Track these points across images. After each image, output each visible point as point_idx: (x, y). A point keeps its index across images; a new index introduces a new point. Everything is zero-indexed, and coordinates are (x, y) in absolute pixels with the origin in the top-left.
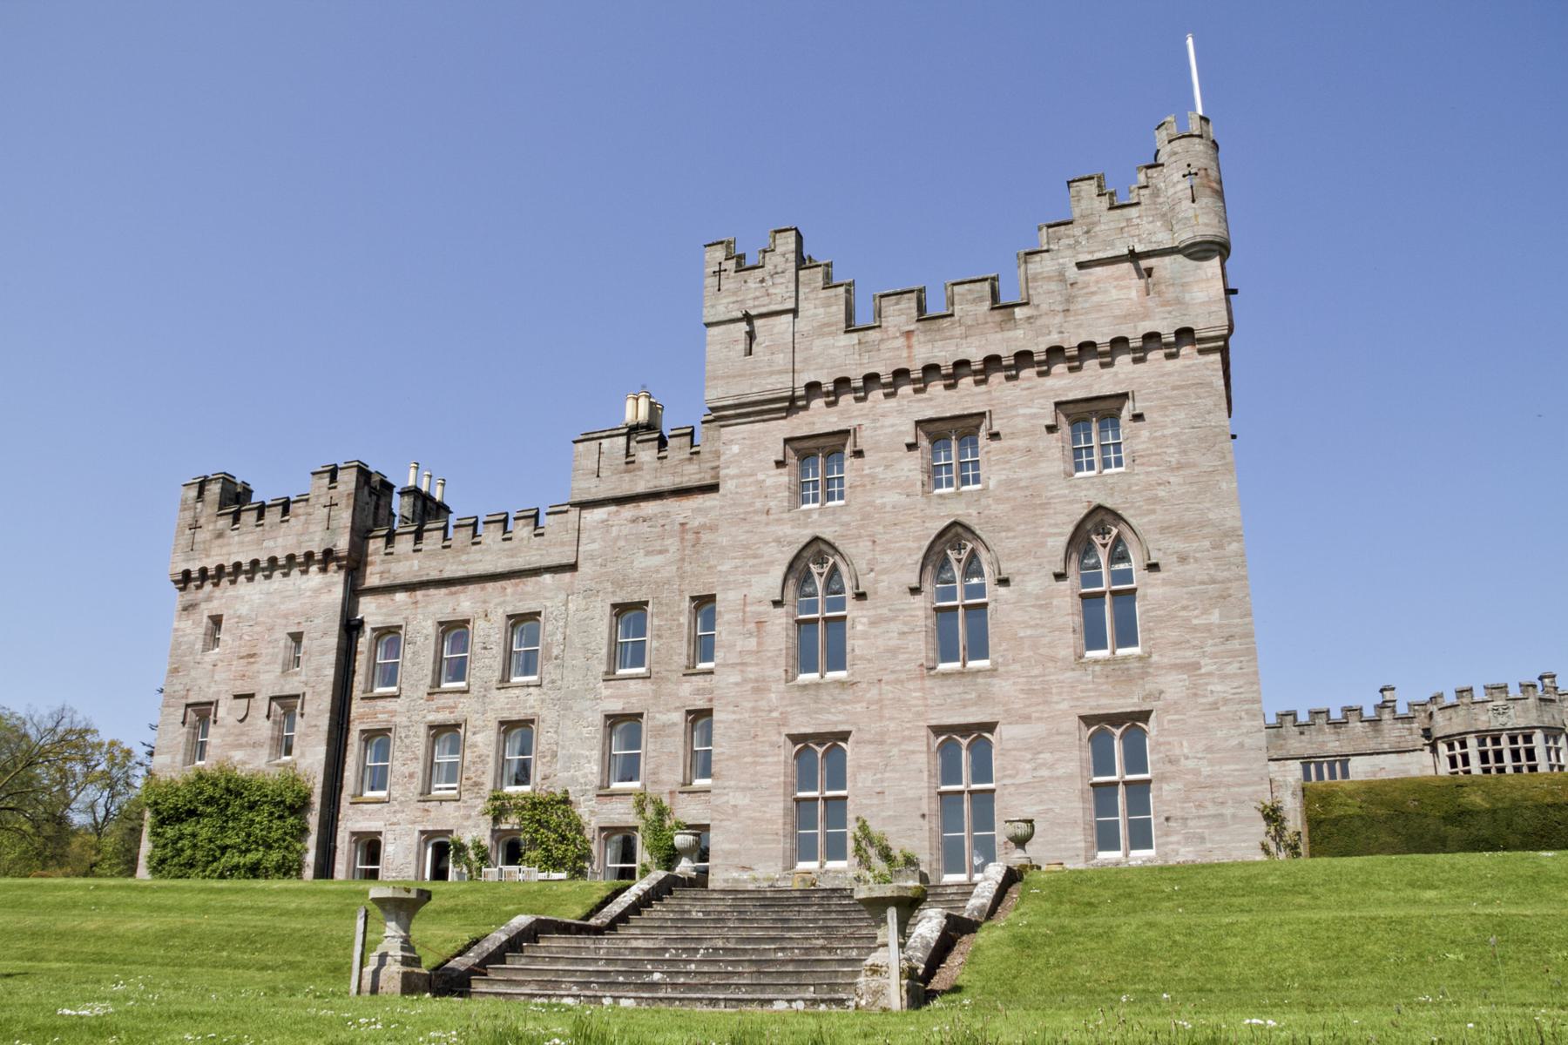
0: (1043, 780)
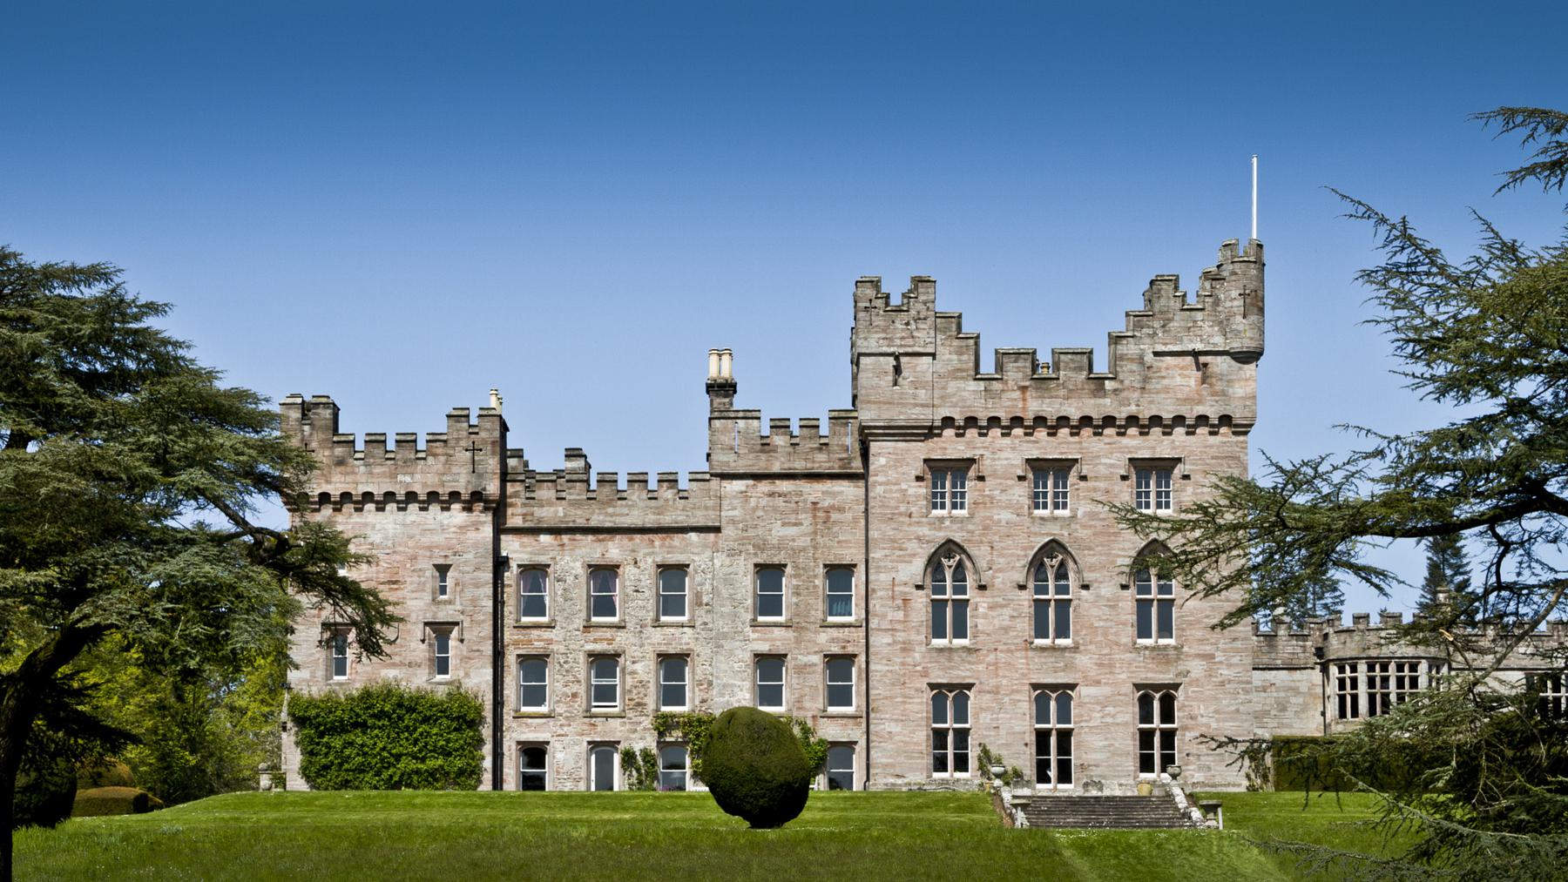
0: (1108, 724)
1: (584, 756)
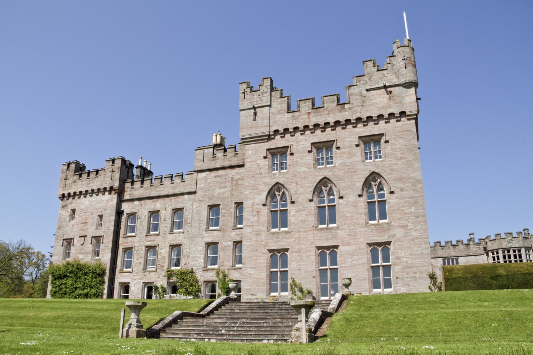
1: (141, 288)
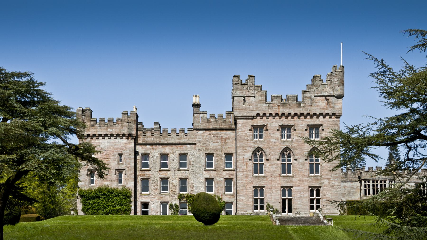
0: (302, 197)
1: (159, 206)
